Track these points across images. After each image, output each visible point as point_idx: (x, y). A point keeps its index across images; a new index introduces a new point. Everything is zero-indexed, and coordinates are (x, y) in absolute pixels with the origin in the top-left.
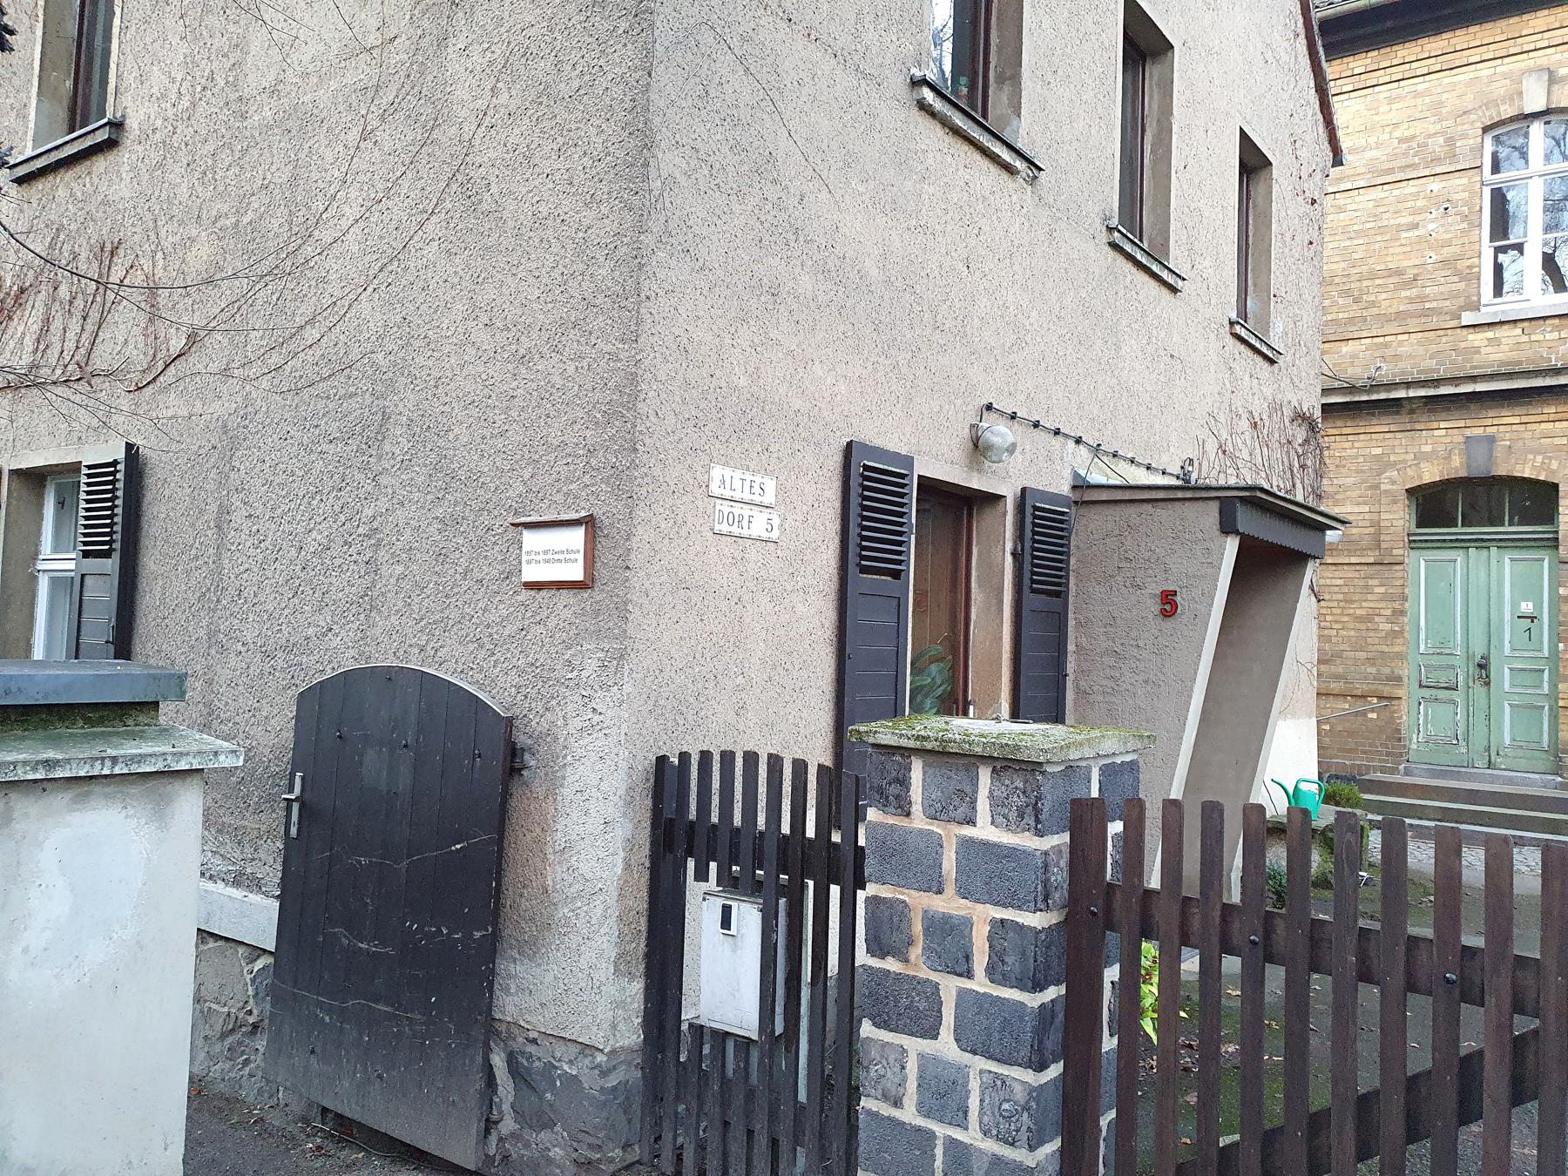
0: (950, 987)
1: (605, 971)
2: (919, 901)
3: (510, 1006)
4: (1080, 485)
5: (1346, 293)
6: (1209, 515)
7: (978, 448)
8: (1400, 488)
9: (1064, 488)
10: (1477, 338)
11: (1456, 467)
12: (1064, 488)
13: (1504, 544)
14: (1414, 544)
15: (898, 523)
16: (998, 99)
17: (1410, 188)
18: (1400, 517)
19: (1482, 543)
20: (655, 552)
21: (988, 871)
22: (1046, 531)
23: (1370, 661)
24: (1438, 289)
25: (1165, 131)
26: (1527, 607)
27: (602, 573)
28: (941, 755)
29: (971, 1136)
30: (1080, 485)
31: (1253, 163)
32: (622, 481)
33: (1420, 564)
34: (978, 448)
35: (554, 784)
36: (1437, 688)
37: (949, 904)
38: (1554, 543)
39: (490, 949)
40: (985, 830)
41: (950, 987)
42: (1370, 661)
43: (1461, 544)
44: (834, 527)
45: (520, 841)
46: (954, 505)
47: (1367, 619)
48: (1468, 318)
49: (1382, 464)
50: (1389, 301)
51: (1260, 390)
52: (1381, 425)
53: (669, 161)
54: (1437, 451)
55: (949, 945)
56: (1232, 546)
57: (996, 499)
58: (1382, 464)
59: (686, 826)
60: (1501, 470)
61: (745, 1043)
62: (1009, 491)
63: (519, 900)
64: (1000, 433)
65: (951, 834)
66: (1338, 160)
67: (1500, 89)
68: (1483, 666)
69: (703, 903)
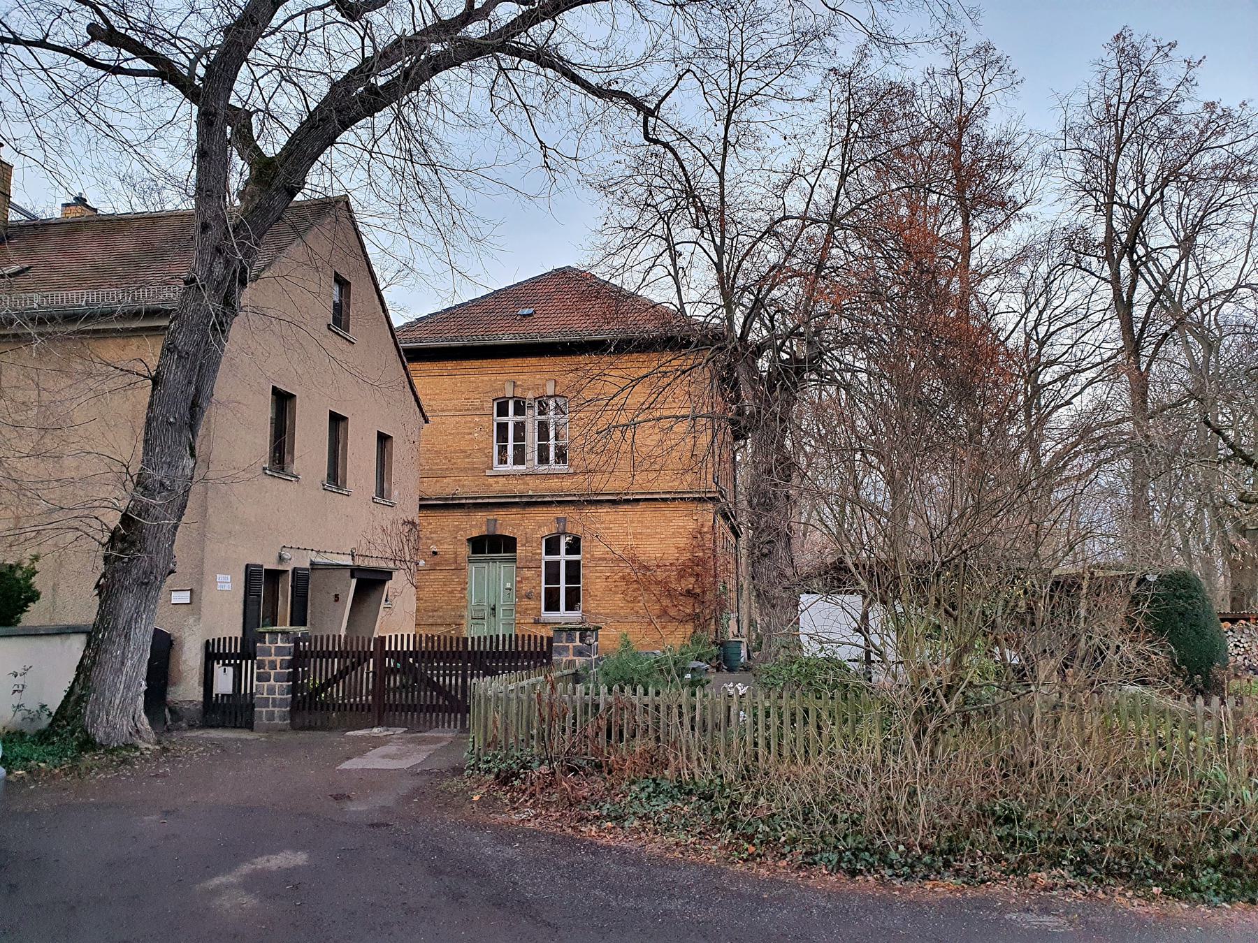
0: (272, 672)
1: (196, 684)
2: (267, 659)
3: (169, 697)
4: (312, 564)
5: (446, 458)
6: (348, 573)
7: (281, 559)
8: (464, 539)
9: (307, 565)
10: (491, 480)
11: (483, 531)
12: (307, 565)
13: (501, 561)
14: (470, 561)
15: (261, 585)
16: (287, 458)
17: (469, 418)
18: (465, 550)
19: (494, 561)
20: (206, 597)
21: (279, 651)
22: (301, 579)
23: (453, 609)
24: (478, 459)
25: (345, 445)
26: (508, 585)
27: (195, 600)
28: (271, 633)
29: (277, 696)
30: (312, 564)
31: (383, 439)
32: (200, 581)
33: (472, 568)
34: (281, 559)
35: (182, 647)
36: (478, 619)
37: (273, 658)
38: (514, 560)
39: (166, 684)
40: (279, 644)
41: (272, 672)
42: (453, 609)
43: (487, 561)
44: (243, 585)
45: (172, 661)
46: (274, 576)
47: (452, 592)
48: (488, 472)
49: (458, 529)
50: (461, 462)
51: (386, 516)
52: (458, 513)
53: (210, 511)
54: (477, 524)
55: (273, 665)
56: (354, 582)
57: (286, 572)
58: (458, 529)
59: (212, 655)
60: (498, 533)
61: (228, 695)
62: (290, 569)
63: (173, 673)
64: (287, 555)
65: (273, 646)
66: (427, 422)
67: (498, 385)
68: (494, 609)
69: (218, 669)
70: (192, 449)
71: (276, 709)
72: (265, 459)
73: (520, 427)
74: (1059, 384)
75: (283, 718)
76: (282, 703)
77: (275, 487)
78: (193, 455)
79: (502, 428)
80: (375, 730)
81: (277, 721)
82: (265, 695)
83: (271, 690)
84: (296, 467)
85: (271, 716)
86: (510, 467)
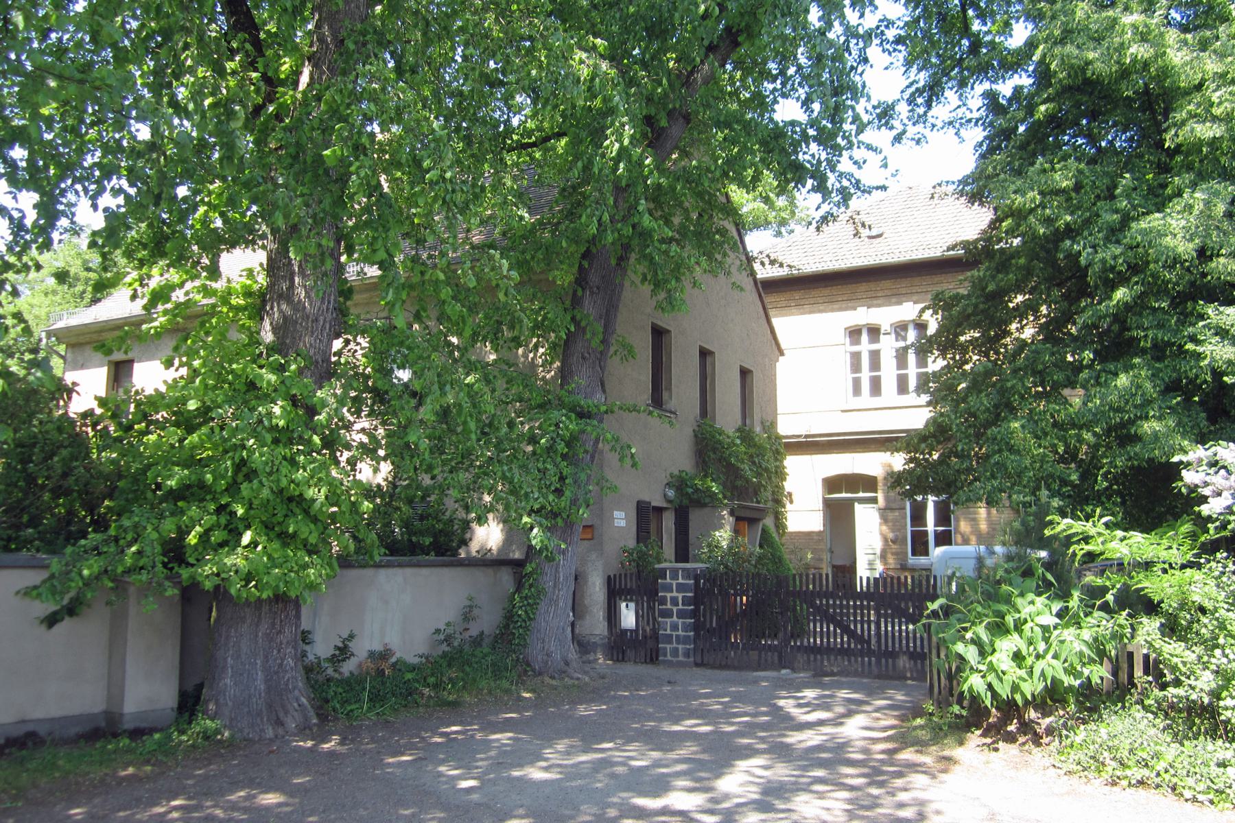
2: (669, 595)
16: (665, 395)
21: (681, 588)
29: (680, 633)
37: (675, 594)
40: (680, 581)
55: (674, 601)
65: (674, 583)
70: (603, 385)
71: (680, 647)
72: (645, 397)
73: (875, 357)
74: (590, 449)
75: (687, 654)
76: (685, 640)
77: (654, 421)
78: (604, 391)
79: (856, 358)
80: (784, 671)
81: (681, 658)
82: (668, 632)
83: (675, 627)
84: (672, 404)
85: (675, 652)
86: (866, 399)
